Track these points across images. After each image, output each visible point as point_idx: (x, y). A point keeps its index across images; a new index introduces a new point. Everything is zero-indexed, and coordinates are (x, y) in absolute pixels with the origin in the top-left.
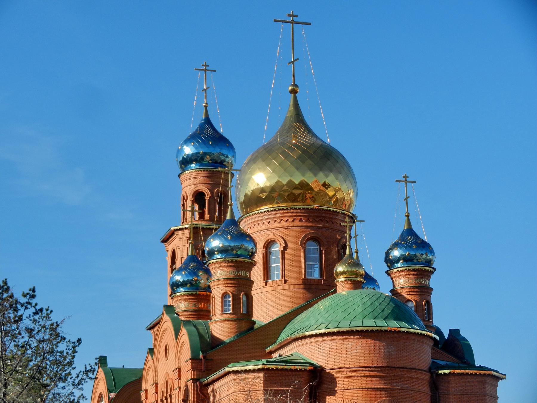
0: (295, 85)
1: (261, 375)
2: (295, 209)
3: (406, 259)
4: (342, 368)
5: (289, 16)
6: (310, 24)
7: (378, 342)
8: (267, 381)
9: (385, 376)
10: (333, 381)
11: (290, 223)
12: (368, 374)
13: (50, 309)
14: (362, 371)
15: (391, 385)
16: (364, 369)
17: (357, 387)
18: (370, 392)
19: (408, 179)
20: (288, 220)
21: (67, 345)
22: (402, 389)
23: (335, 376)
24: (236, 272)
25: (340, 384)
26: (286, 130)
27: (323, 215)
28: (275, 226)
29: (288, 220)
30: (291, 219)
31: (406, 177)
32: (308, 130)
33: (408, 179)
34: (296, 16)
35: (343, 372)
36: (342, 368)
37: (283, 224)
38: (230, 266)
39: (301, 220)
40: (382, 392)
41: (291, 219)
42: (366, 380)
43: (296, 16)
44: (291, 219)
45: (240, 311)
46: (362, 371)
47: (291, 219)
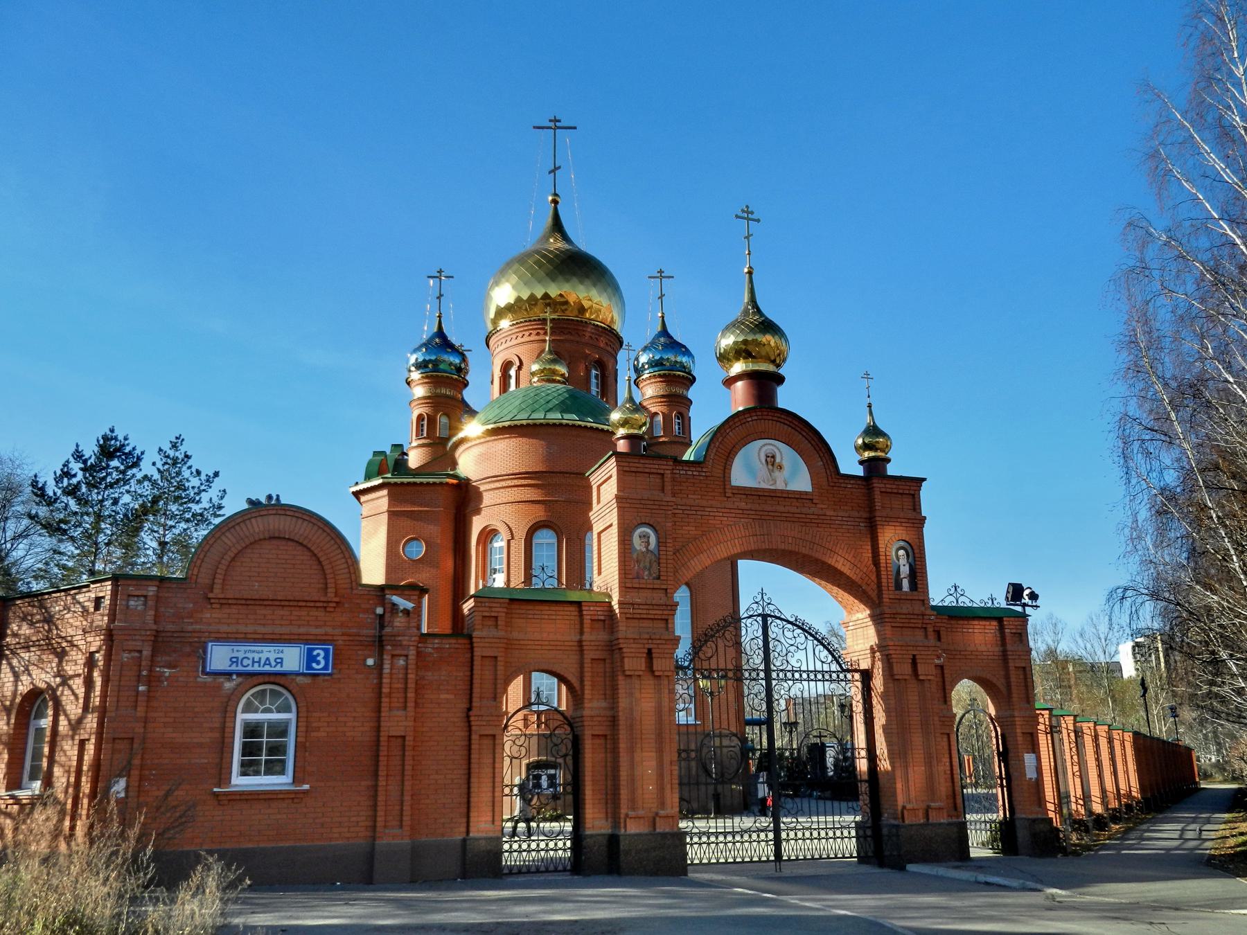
0: (556, 194)
1: (385, 492)
2: (530, 321)
3: (654, 364)
4: (488, 478)
5: (551, 121)
6: (575, 128)
7: (534, 441)
8: (391, 496)
9: (543, 484)
10: (478, 496)
11: (526, 339)
12: (519, 483)
13: (182, 438)
14: (512, 479)
15: (552, 496)
16: (507, 477)
17: (505, 500)
18: (521, 505)
19: (663, 275)
20: (531, 334)
21: (68, 461)
22: (568, 502)
23: (482, 488)
24: (435, 388)
25: (487, 499)
26: (746, 312)
27: (565, 326)
28: (523, 340)
29: (531, 334)
30: (527, 333)
31: (661, 272)
32: (565, 238)
33: (663, 275)
34: (559, 121)
35: (489, 482)
36: (488, 478)
37: (520, 340)
38: (426, 383)
39: (538, 334)
40: (537, 506)
41: (527, 333)
42: (733, 519)
43: (559, 121)
44: (527, 333)
45: (435, 432)
46: (512, 479)
47: (527, 333)
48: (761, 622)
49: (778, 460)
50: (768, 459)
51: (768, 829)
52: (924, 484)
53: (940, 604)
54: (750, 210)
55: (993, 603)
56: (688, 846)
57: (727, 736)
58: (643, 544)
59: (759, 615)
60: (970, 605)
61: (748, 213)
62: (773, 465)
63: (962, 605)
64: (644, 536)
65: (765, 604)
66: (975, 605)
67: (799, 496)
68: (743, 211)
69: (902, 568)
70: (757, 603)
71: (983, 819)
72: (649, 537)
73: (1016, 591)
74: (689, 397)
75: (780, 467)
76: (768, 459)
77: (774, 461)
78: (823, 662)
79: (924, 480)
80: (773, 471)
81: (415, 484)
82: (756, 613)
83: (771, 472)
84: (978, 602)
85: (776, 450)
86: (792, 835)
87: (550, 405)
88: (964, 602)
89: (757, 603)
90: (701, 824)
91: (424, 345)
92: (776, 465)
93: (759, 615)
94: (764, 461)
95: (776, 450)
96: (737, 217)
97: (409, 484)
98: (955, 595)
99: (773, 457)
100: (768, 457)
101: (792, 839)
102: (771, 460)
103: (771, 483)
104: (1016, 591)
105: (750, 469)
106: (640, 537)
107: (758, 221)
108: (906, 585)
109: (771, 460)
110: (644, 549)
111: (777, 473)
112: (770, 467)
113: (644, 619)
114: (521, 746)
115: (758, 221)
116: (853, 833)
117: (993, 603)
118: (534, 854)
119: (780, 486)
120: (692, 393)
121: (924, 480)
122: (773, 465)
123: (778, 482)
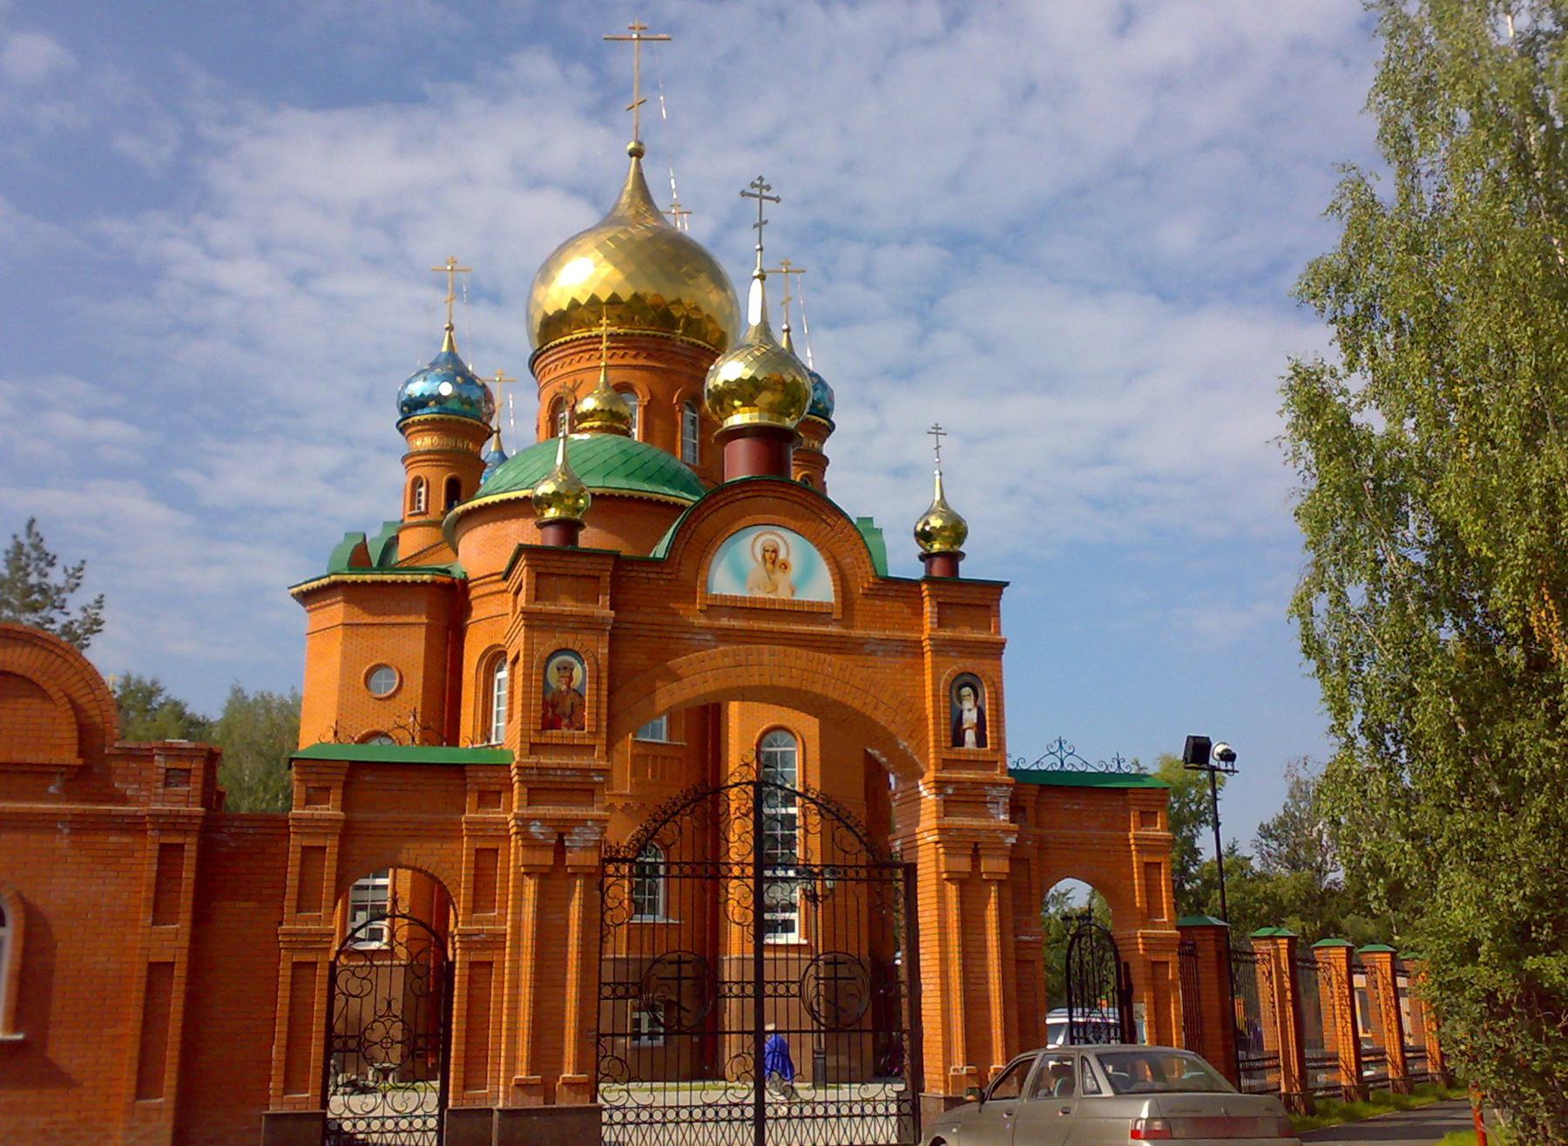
28: (634, 362)
48: (752, 794)
49: (782, 556)
50: (768, 555)
51: (746, 1102)
52: (1005, 590)
53: (1035, 768)
54: (764, 183)
55: (1119, 766)
56: (604, 1128)
57: (845, 963)
58: (563, 680)
59: (749, 783)
60: (1082, 769)
61: (762, 187)
62: (774, 563)
63: (1069, 769)
64: (565, 668)
65: (1064, 754)
66: (1090, 770)
67: (812, 613)
68: (753, 185)
69: (966, 715)
70: (747, 764)
71: (882, 1097)
72: (572, 669)
73: (1198, 750)
74: (824, 453)
75: (785, 566)
76: (768, 555)
77: (776, 556)
78: (846, 852)
79: (1007, 584)
80: (773, 572)
81: (383, 583)
82: (744, 780)
83: (770, 573)
84: (1096, 766)
85: (781, 543)
86: (618, 1116)
87: (590, 466)
88: (1073, 764)
89: (747, 764)
90: (641, 1093)
91: (792, 351)
92: (778, 563)
93: (749, 783)
94: (760, 558)
95: (781, 543)
96: (743, 194)
97: (374, 583)
98: (1058, 754)
99: (775, 551)
100: (766, 551)
101: (671, 1122)
102: (772, 558)
103: (770, 589)
104: (1198, 750)
105: (739, 573)
106: (558, 669)
107: (777, 200)
108: (970, 737)
109: (772, 558)
110: (564, 687)
111: (779, 576)
112: (769, 566)
113: (565, 789)
114: (364, 979)
115: (777, 200)
116: (893, 1108)
117: (1119, 766)
118: (389, 1136)
119: (783, 594)
120: (829, 448)
121: (1007, 584)
122: (774, 563)
123: (780, 589)
